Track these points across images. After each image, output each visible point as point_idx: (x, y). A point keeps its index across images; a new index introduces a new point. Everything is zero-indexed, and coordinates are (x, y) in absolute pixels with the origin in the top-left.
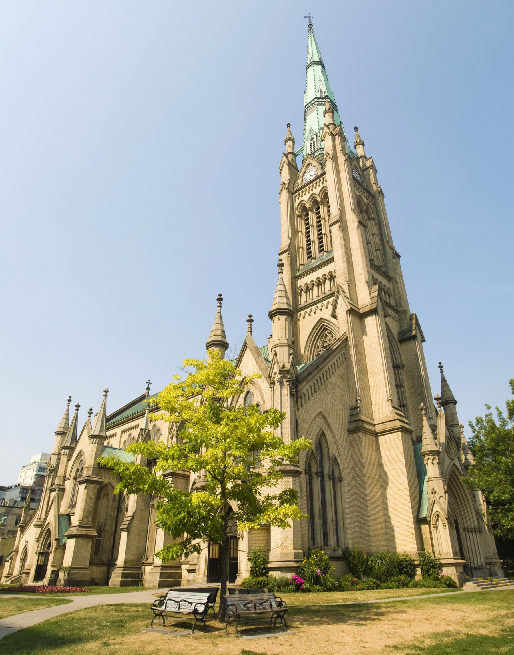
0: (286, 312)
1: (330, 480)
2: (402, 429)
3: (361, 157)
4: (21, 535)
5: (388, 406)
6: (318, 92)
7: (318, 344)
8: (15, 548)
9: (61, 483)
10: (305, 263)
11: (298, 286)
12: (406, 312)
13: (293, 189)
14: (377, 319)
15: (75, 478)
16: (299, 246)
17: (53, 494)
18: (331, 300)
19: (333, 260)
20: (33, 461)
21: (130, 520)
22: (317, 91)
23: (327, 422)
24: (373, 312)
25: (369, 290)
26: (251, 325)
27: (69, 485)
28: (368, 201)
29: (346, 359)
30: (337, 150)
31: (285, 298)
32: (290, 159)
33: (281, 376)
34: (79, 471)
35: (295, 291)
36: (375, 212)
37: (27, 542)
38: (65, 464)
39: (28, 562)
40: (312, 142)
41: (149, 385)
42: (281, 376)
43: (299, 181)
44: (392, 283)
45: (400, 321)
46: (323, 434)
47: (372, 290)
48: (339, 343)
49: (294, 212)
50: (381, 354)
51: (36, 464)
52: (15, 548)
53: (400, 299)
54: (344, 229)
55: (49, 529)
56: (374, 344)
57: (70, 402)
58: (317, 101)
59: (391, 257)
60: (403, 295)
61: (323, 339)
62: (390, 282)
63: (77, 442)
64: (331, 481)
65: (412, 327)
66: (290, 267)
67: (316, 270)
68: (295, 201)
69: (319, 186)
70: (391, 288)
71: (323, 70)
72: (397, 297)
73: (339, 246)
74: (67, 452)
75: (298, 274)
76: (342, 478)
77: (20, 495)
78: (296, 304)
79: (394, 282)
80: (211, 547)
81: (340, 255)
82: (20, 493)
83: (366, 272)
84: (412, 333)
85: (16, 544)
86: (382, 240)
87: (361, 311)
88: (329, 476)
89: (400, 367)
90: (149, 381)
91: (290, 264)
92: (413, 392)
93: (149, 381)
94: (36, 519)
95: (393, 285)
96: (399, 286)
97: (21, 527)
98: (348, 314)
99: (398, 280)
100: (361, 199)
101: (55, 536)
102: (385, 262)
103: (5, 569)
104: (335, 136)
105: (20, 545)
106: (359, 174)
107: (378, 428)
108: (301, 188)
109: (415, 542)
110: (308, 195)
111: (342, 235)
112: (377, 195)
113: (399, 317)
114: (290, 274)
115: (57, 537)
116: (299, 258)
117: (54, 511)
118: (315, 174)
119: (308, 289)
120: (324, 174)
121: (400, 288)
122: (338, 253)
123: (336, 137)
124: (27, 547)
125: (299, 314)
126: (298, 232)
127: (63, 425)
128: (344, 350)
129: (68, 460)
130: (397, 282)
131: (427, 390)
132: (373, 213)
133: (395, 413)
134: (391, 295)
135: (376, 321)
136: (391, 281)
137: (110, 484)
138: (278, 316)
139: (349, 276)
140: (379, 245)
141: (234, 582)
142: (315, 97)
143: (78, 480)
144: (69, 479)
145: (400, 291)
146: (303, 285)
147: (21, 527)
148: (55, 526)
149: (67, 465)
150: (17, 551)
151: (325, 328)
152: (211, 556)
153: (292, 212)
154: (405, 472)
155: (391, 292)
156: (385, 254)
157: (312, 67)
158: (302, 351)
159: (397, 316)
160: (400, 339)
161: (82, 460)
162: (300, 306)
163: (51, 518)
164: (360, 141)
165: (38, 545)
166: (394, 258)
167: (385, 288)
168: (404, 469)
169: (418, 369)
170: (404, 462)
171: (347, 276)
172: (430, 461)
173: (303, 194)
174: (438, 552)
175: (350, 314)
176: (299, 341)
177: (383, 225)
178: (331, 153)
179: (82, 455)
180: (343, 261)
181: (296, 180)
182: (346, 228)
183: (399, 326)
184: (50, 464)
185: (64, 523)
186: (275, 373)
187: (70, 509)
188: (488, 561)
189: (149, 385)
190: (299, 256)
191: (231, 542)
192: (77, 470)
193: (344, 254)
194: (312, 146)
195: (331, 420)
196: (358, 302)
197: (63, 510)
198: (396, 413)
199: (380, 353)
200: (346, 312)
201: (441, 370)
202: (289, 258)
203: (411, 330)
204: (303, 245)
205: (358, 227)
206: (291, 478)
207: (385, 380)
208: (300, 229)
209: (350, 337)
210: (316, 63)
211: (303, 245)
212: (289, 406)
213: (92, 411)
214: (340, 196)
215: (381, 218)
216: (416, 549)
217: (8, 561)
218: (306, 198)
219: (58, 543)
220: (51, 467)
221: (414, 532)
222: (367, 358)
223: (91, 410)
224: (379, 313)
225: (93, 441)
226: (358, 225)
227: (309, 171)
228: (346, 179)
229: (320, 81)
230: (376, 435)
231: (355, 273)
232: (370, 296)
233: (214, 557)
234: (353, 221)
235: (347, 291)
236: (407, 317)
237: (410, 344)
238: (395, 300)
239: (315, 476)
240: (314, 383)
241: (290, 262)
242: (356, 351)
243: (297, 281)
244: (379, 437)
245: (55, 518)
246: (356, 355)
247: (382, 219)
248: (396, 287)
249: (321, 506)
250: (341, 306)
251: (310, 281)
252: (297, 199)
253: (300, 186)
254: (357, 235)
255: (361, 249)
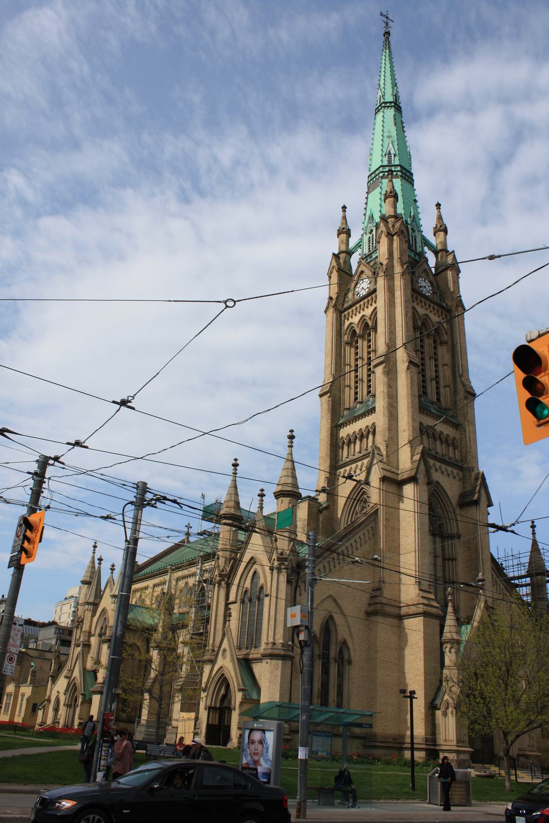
0: (290, 494)
1: (335, 663)
2: (425, 614)
3: (441, 250)
4: (52, 684)
5: (415, 588)
6: (385, 156)
7: (357, 509)
8: (47, 697)
9: (87, 639)
10: (351, 406)
11: (340, 437)
12: (471, 469)
13: (343, 305)
14: (416, 488)
15: (100, 635)
16: (345, 384)
17: (79, 649)
18: (366, 461)
19: (375, 411)
20: (69, 594)
21: (153, 682)
22: (384, 155)
23: (338, 605)
24: (413, 479)
25: (411, 452)
26: (262, 500)
27: (94, 641)
28: (438, 320)
29: (374, 535)
30: (394, 257)
31: (291, 477)
32: (342, 261)
33: (279, 562)
34: (104, 628)
35: (336, 443)
36: (449, 333)
37: (59, 693)
38: (89, 620)
39: (60, 713)
40: (371, 236)
41: (188, 529)
42: (279, 562)
43: (350, 295)
44: (460, 431)
45: (463, 480)
46: (331, 617)
47: (416, 451)
48: (363, 519)
49: (341, 337)
50: (415, 530)
51: (73, 600)
52: (47, 697)
53: (467, 453)
54: (391, 373)
55: (75, 684)
56: (409, 517)
57: (96, 549)
58: (381, 172)
59: (462, 396)
60: (470, 448)
61: (362, 504)
62: (457, 430)
63: (101, 599)
64: (336, 664)
65: (475, 489)
66: (330, 413)
67: (359, 418)
68: (344, 322)
69: (371, 305)
70: (458, 437)
71: (398, 115)
72: (463, 450)
73: (382, 395)
74: (91, 607)
75: (341, 421)
76: (351, 661)
77: (56, 636)
78: (335, 460)
79: (462, 430)
80: (211, 714)
81: (382, 406)
82: (55, 633)
83: (411, 428)
84: (474, 497)
85: (48, 694)
86: (454, 372)
87: (400, 478)
88: (334, 658)
89: (455, 537)
90: (189, 524)
91: (330, 409)
92: (468, 567)
93: (189, 524)
94: (66, 671)
95: (461, 434)
96: (468, 436)
97: (52, 676)
98: (381, 483)
99: (467, 428)
100: (428, 319)
101: (81, 691)
102: (455, 403)
103: (38, 717)
104: (393, 236)
105: (52, 695)
106: (431, 282)
107: (404, 611)
108: (351, 307)
109: (424, 727)
110: (359, 316)
111: (386, 380)
112: (454, 309)
113: (463, 475)
114: (330, 423)
115: (83, 692)
116: (344, 400)
117: (80, 667)
118: (368, 288)
119: (350, 441)
120: (375, 291)
121: (468, 438)
122: (380, 403)
123: (395, 237)
124: (59, 697)
125: (338, 471)
126: (345, 366)
127: (89, 574)
128: (372, 524)
129: (93, 615)
130: (465, 431)
131: (483, 564)
132: (447, 334)
133: (420, 596)
134: (457, 447)
135: (414, 491)
136: (459, 428)
137: (135, 644)
138: (282, 498)
139: (389, 433)
140: (449, 380)
141: (226, 746)
142: (380, 165)
143: (103, 638)
144: (94, 635)
145: (468, 442)
146: (345, 436)
147: (52, 676)
148: (81, 682)
149: (91, 621)
150: (49, 701)
151: (364, 492)
152: (210, 723)
153: (339, 338)
154: (423, 658)
155: (457, 443)
156: (455, 392)
157: (381, 111)
158: (339, 516)
159: (461, 474)
160: (460, 503)
161: (106, 618)
162: (341, 463)
163: (77, 673)
164: (441, 226)
165: (66, 698)
166: (466, 398)
167: (448, 439)
168: (422, 655)
169: (476, 539)
170: (423, 649)
171: (387, 434)
172: (447, 650)
173: (356, 312)
174: (444, 738)
175: (383, 482)
176: (336, 505)
177: (457, 352)
178: (385, 262)
179: (105, 613)
180: (384, 415)
181: (346, 294)
182: (394, 369)
183: (462, 487)
184: (77, 615)
185: (90, 678)
186: (274, 560)
187: (96, 666)
188: (521, 753)
189: (188, 529)
190: (344, 397)
191: (225, 712)
192: (102, 628)
193: (386, 406)
194: (371, 242)
195: (344, 604)
196: (398, 465)
197: (89, 665)
198: (422, 597)
199: (414, 529)
200: (379, 480)
201: (533, 531)
202: (331, 402)
203: (473, 493)
204: (350, 383)
205: (408, 369)
206: (281, 661)
207: (415, 559)
208: (347, 361)
209: (380, 509)
210: (388, 105)
211: (350, 383)
212: (285, 593)
213: (114, 567)
214: (390, 325)
215: (455, 342)
216: (424, 734)
217: (41, 709)
218: (356, 319)
219: (84, 698)
220: (79, 618)
221: (424, 718)
222: (402, 533)
223: (113, 566)
224: (419, 480)
225: (115, 601)
226: (408, 366)
227: (361, 282)
228: (400, 301)
229: (389, 137)
230: (400, 618)
231: (399, 428)
232: (412, 459)
233: (213, 723)
234: (403, 361)
235: (384, 453)
236: (471, 476)
237: (472, 511)
238: (461, 453)
239: (317, 659)
240: (324, 566)
241: (330, 407)
242: (385, 526)
243: (340, 429)
244: (405, 620)
245: (80, 673)
246: (386, 531)
247: (457, 343)
248: (463, 436)
249: (320, 687)
250: (375, 472)
251: (352, 433)
252: (346, 320)
253: (350, 303)
254: (405, 379)
255: (408, 399)
